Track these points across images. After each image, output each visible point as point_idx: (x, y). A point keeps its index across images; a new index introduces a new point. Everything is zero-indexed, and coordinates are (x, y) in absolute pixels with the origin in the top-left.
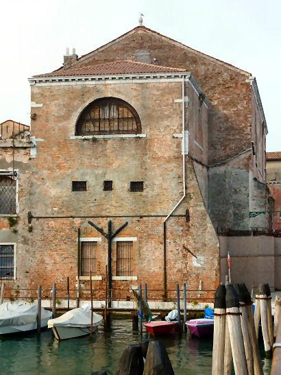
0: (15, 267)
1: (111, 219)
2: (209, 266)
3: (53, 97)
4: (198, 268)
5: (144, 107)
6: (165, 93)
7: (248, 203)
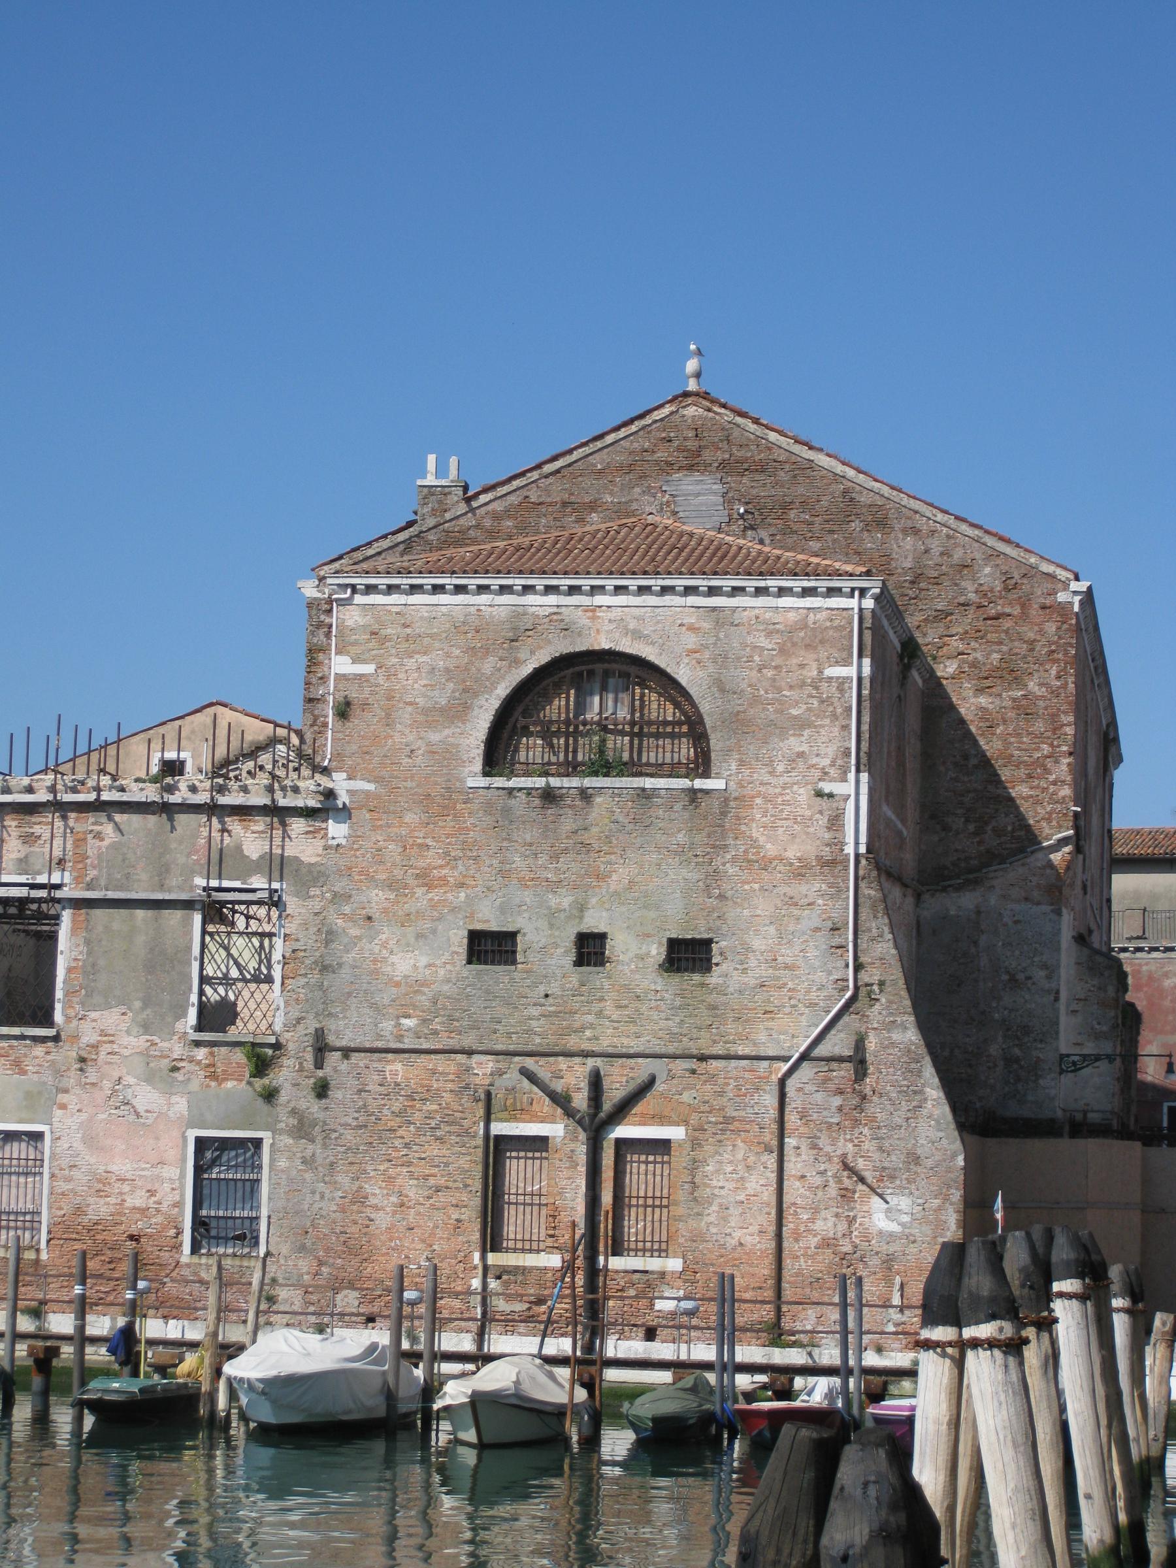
0: (264, 1212)
1: (598, 1062)
2: (927, 1230)
3: (413, 643)
4: (891, 1237)
5: (722, 690)
6: (794, 644)
7: (1057, 1023)
